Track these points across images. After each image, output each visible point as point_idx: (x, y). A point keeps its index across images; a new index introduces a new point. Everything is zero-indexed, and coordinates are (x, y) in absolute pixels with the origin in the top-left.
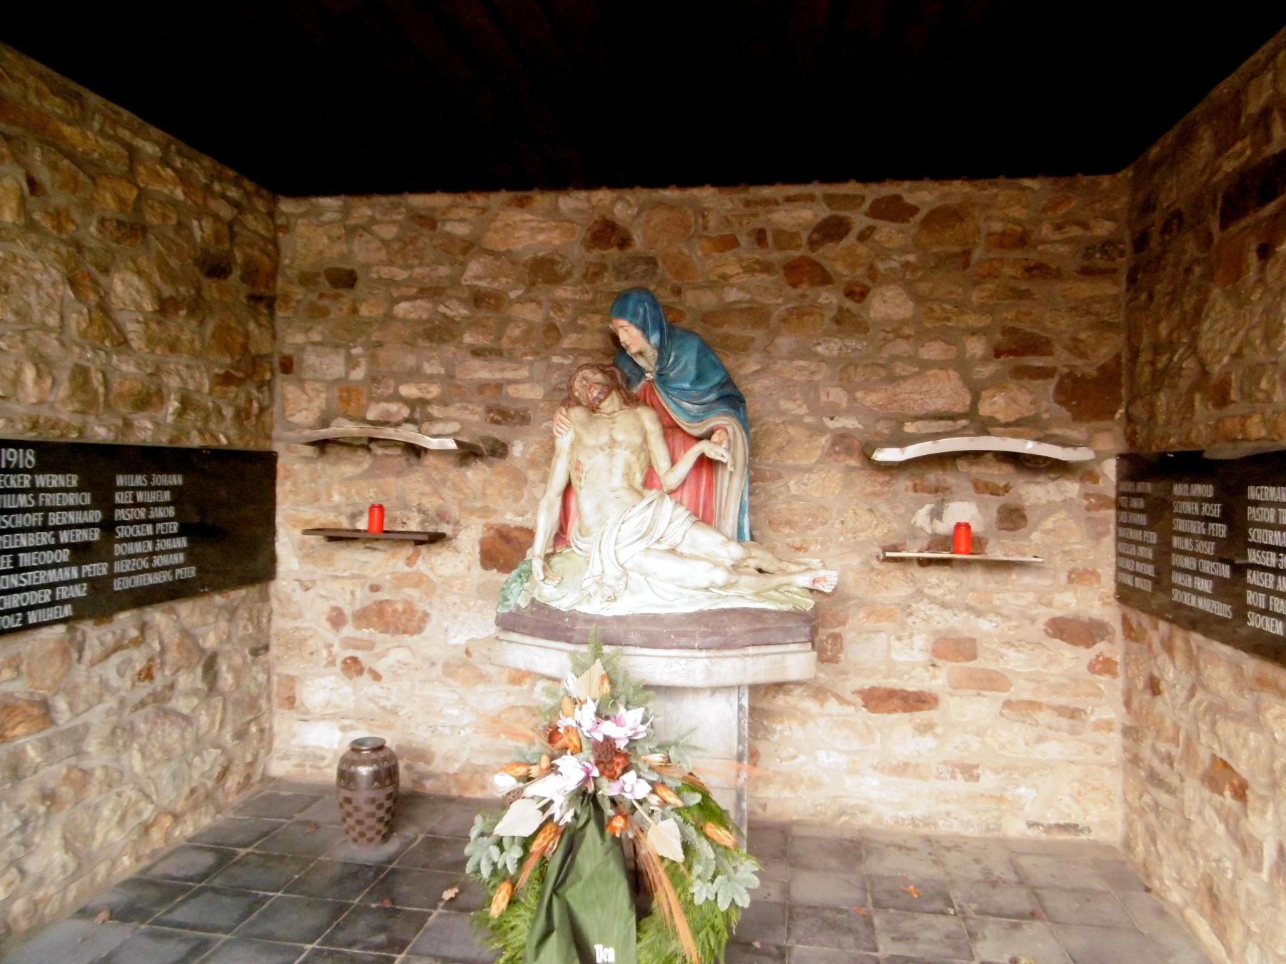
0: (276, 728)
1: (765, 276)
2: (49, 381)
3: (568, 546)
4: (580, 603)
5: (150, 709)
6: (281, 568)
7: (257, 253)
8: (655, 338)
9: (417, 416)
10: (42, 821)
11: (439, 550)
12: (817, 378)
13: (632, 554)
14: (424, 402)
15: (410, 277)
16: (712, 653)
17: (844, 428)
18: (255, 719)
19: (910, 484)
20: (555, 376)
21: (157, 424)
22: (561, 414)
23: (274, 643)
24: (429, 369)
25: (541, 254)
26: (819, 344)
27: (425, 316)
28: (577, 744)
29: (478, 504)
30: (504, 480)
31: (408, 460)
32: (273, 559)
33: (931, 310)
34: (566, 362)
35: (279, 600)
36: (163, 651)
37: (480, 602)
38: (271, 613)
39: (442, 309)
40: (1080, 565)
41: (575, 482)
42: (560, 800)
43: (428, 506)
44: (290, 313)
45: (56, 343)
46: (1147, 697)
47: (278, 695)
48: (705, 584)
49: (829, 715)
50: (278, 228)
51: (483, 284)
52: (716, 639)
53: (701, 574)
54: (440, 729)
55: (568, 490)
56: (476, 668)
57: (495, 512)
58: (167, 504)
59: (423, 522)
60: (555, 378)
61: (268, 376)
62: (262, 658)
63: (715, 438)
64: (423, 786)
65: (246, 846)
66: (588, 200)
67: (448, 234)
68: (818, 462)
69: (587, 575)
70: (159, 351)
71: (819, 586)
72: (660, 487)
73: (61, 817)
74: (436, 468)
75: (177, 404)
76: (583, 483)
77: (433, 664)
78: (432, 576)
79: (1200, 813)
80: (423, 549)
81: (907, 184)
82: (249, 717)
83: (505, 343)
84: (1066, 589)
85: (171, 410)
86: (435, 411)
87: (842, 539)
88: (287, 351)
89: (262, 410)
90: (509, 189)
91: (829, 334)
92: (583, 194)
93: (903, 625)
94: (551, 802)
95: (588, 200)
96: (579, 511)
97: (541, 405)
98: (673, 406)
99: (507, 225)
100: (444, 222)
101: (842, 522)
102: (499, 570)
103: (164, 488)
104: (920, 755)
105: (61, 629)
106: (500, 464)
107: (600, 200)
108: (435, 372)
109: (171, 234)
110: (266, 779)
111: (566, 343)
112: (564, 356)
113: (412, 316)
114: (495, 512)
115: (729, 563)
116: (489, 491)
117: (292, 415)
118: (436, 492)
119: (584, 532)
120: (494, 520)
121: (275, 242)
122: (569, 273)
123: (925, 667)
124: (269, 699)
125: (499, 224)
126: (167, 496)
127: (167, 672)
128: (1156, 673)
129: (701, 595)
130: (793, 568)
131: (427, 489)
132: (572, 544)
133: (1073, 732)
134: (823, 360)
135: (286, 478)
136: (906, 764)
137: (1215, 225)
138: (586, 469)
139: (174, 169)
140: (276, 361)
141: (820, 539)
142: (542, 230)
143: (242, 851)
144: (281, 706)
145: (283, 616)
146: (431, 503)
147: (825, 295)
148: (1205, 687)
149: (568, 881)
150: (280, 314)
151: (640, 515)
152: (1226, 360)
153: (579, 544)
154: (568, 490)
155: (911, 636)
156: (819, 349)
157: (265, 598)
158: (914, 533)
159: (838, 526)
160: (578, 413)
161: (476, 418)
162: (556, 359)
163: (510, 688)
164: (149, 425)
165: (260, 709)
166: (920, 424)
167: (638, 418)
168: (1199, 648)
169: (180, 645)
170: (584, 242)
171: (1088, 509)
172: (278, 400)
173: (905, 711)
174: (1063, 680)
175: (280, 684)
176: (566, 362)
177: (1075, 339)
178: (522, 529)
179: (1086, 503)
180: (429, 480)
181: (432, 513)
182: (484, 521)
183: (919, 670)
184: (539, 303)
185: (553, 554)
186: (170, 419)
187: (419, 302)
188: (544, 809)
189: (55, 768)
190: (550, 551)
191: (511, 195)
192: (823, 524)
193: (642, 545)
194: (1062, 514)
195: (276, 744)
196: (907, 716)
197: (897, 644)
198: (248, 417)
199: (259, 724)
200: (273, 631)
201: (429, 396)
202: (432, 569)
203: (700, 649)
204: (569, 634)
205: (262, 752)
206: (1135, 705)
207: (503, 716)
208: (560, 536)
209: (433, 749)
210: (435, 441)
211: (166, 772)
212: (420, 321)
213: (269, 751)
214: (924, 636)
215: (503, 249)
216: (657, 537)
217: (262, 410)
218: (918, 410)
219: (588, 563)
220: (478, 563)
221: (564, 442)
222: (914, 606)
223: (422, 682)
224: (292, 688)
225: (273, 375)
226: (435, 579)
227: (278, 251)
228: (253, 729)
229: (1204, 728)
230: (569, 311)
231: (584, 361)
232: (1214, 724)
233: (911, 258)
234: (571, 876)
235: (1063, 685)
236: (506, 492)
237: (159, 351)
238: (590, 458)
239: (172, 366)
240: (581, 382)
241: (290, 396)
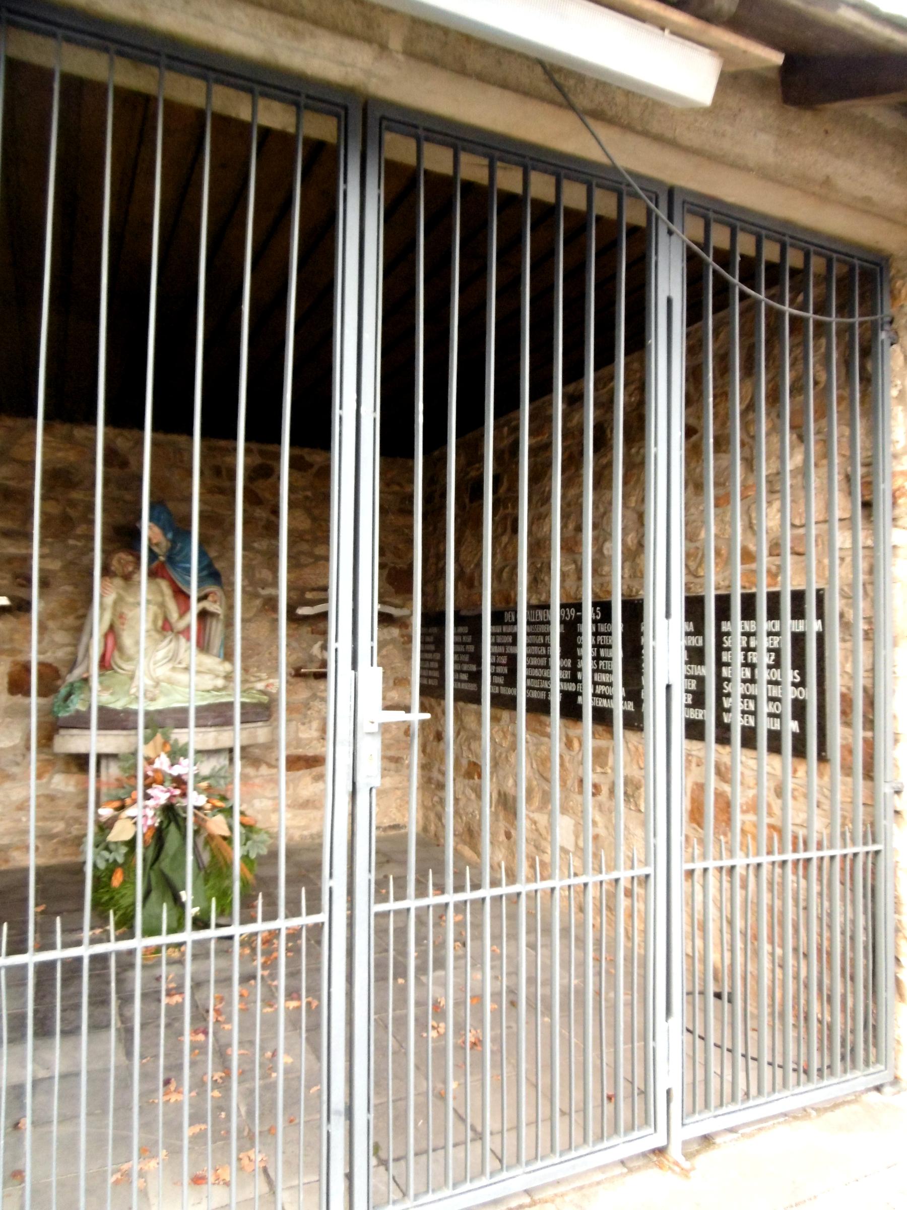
1: (221, 496)
4: (131, 703)
8: (170, 536)
12: (254, 562)
13: (163, 671)
16: (218, 728)
17: (270, 594)
19: (309, 629)
25: (59, 466)
26: (255, 541)
29: (7, 647)
33: (321, 526)
34: (79, 544)
37: (8, 720)
40: (399, 675)
46: (435, 743)
48: (210, 687)
49: (262, 776)
51: (12, 483)
52: (218, 720)
53: (209, 682)
57: (20, 652)
60: (70, 556)
63: (210, 598)
68: (255, 615)
71: (269, 689)
72: (172, 630)
76: (125, 627)
79: (464, 793)
81: (306, 450)
84: (393, 689)
87: (269, 664)
91: (262, 536)
93: (305, 716)
97: (60, 574)
98: (180, 579)
101: (270, 653)
104: (316, 795)
114: (20, 652)
115: (223, 674)
116: (16, 636)
123: (318, 740)
128: (440, 729)
129: (207, 695)
130: (252, 679)
133: (397, 771)
134: (257, 551)
136: (308, 801)
137: (467, 501)
141: (257, 664)
142: (59, 450)
147: (258, 511)
148: (464, 728)
151: (165, 649)
152: (472, 566)
155: (310, 722)
156: (256, 545)
158: (311, 659)
159: (267, 655)
161: (5, 582)
162: (71, 542)
166: (315, 593)
167: (159, 585)
168: (462, 709)
171: (403, 643)
173: (307, 768)
174: (392, 742)
177: (396, 547)
179: (402, 640)
183: (315, 742)
184: (57, 500)
192: (258, 654)
193: (170, 665)
194: (391, 647)
196: (308, 771)
197: (302, 728)
203: (211, 726)
204: (125, 723)
206: (428, 750)
214: (317, 721)
216: (178, 661)
218: (313, 585)
220: (6, 691)
222: (311, 703)
229: (465, 748)
232: (469, 745)
233: (309, 494)
235: (392, 744)
238: (131, 610)
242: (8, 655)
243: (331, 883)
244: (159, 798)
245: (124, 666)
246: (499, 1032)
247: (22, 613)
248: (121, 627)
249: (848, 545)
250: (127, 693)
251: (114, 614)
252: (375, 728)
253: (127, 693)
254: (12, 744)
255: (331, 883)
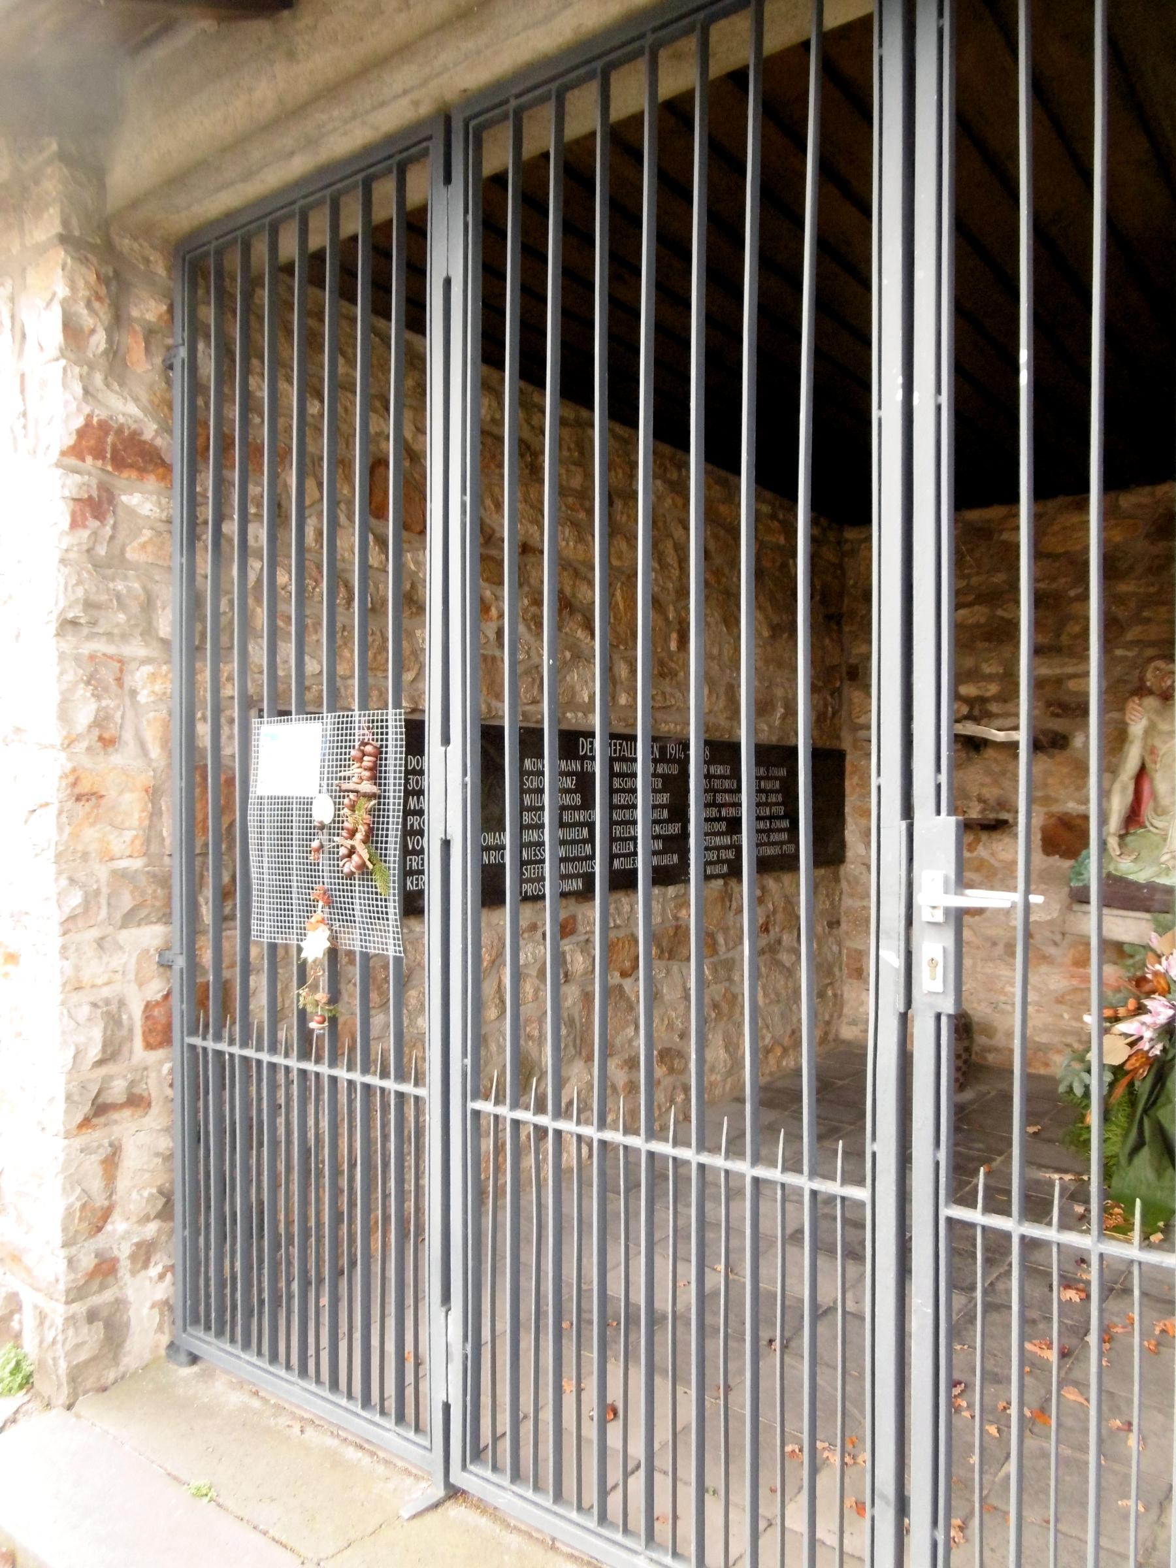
0: (846, 996)
2: (715, 696)
3: (1143, 826)
4: (1158, 875)
5: (767, 956)
6: (850, 854)
7: (829, 578)
9: (976, 712)
10: (713, 1024)
11: (999, 837)
14: (983, 700)
15: (968, 585)
18: (831, 984)
20: (1119, 668)
21: (770, 727)
22: (1133, 705)
23: (843, 920)
24: (987, 669)
27: (983, 620)
28: (1165, 986)
30: (1065, 770)
31: (967, 753)
32: (842, 845)
34: (1130, 654)
35: (849, 882)
36: (774, 912)
38: (841, 893)
39: (1000, 612)
41: (1149, 765)
42: (1148, 1034)
43: (988, 796)
44: (854, 628)
45: (717, 668)
47: (848, 965)
50: (844, 554)
54: (1003, 1006)
55: (1141, 774)
56: (1039, 949)
57: (1056, 800)
58: (777, 792)
59: (983, 811)
61: (838, 684)
62: (835, 931)
64: (985, 1059)
65: (840, 1079)
66: (1153, 494)
67: (1003, 542)
69: (1166, 850)
70: (771, 668)
73: (722, 1024)
74: (996, 760)
75: (782, 710)
76: (1158, 766)
77: (994, 944)
78: (992, 861)
80: (984, 836)
82: (828, 981)
83: (1065, 640)
85: (779, 715)
86: (994, 708)
88: (853, 661)
89: (834, 713)
90: (1067, 494)
92: (1148, 489)
94: (1141, 1038)
95: (1153, 494)
96: (1154, 795)
99: (1065, 528)
100: (1001, 532)
102: (1061, 856)
103: (776, 778)
105: (720, 882)
106: (1060, 756)
107: (1166, 493)
108: (994, 671)
109: (777, 574)
110: (837, 1039)
111: (1129, 636)
112: (1128, 649)
113: (970, 621)
114: (1056, 800)
116: (1050, 781)
117: (858, 717)
118: (996, 782)
119: (1160, 811)
120: (1056, 809)
121: (840, 566)
122: (1131, 568)
124: (841, 969)
125: (1056, 528)
126: (777, 785)
127: (777, 929)
131: (988, 780)
132: (1147, 824)
135: (854, 773)
138: (1161, 753)
139: (778, 520)
140: (844, 669)
143: (840, 1083)
144: (850, 976)
145: (852, 896)
146: (991, 793)
149: (1159, 1104)
150: (846, 629)
153: (1155, 822)
154: (1141, 774)
157: (837, 880)
160: (1151, 702)
163: (1074, 969)
164: (766, 728)
165: (834, 975)
169: (784, 909)
170: (1147, 536)
172: (845, 707)
175: (848, 956)
176: (1130, 654)
178: (1079, 816)
180: (989, 773)
181: (992, 802)
182: (1045, 809)
185: (1127, 834)
186: (777, 723)
187: (976, 608)
188: (1131, 1045)
189: (719, 986)
190: (1123, 832)
191: (1070, 499)
195: (845, 1010)
198: (825, 720)
199: (833, 989)
200: (843, 908)
201: (988, 694)
202: (993, 854)
205: (836, 1015)
207: (1068, 997)
208: (1133, 817)
209: (995, 1024)
210: (1002, 734)
211: (776, 1009)
212: (977, 625)
213: (840, 1016)
215: (1060, 550)
217: (834, 713)
219: (1165, 840)
221: (1137, 728)
223: (984, 960)
224: (860, 961)
225: (842, 682)
226: (997, 865)
227: (844, 574)
228: (830, 993)
230: (1133, 605)
231: (1150, 652)
234: (1162, 1099)
236: (1067, 781)
237: (771, 668)
238: (1165, 742)
239: (778, 680)
240: (1154, 672)
241: (856, 700)
242: (1042, 806)
243: (876, 1147)
244: (1158, 1014)
245: (1156, 823)
246: (987, 1477)
247: (1056, 751)
248: (1153, 766)
249: (252, 528)
250: (1156, 861)
251: (1144, 748)
252: (939, 917)
253: (1156, 861)
254: (1049, 918)
255: (876, 1147)
